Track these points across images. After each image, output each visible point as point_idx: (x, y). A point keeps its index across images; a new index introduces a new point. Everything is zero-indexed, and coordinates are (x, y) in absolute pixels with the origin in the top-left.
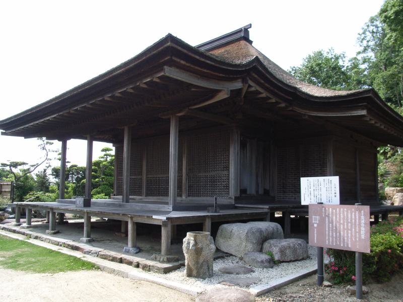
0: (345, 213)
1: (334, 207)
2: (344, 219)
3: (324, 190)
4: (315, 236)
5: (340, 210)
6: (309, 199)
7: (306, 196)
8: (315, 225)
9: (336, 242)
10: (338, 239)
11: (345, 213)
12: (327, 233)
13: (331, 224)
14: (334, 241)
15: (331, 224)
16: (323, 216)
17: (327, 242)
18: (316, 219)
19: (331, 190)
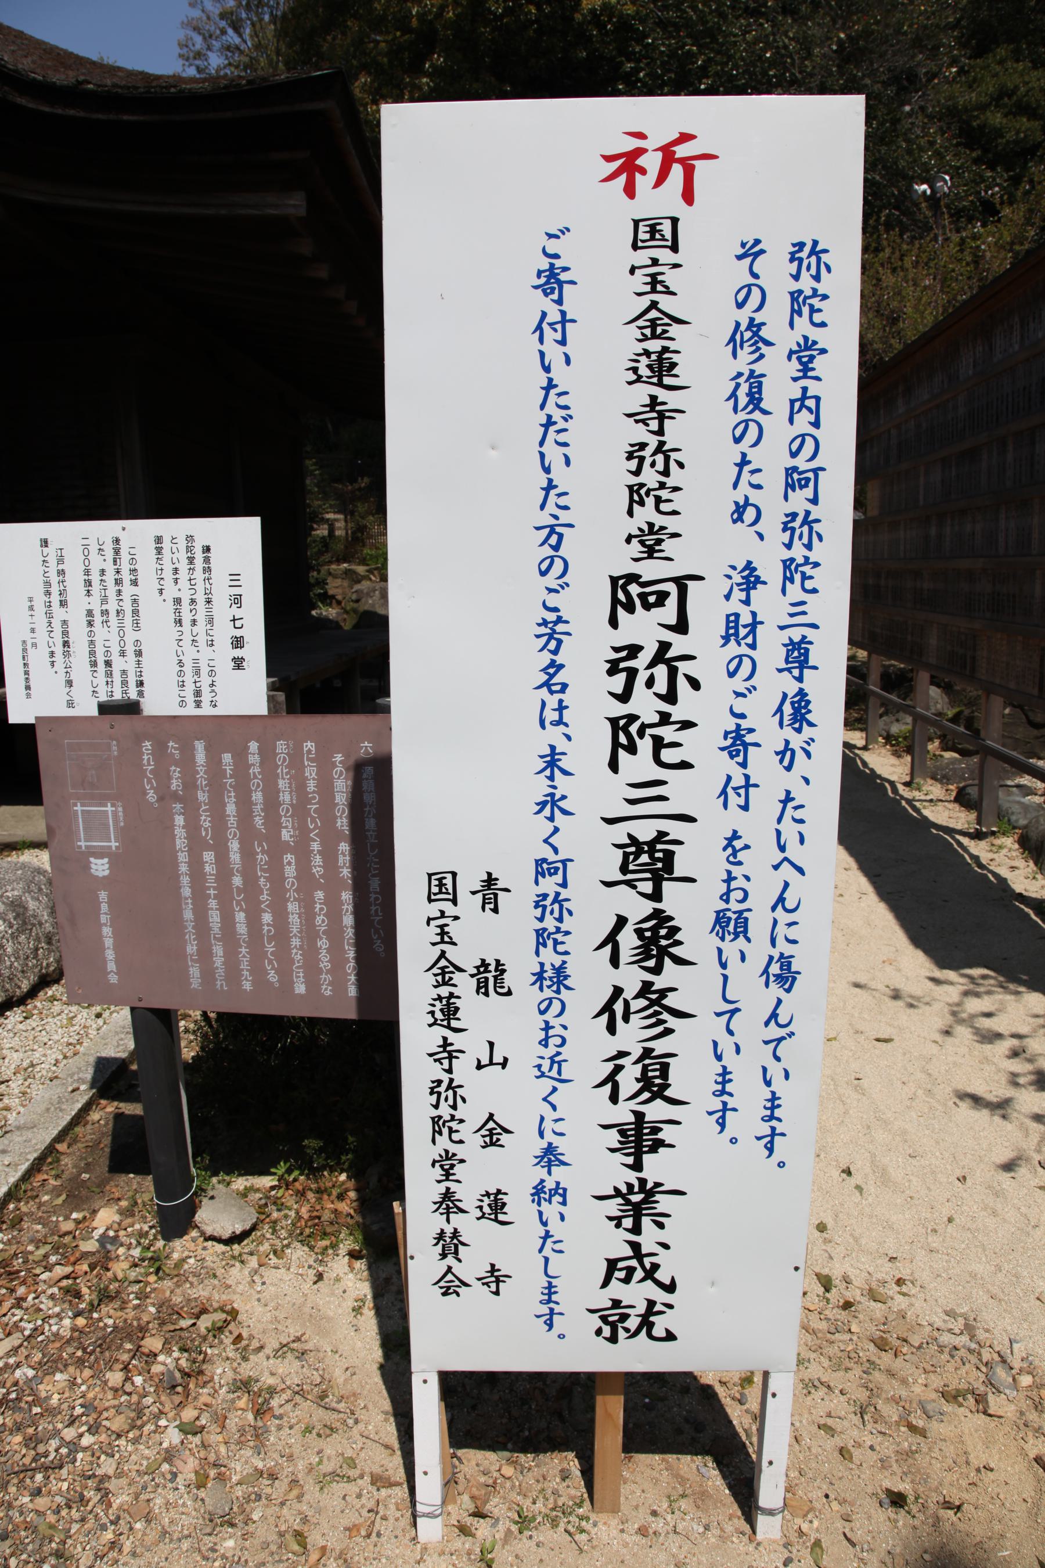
0: (311, 772)
1: (225, 731)
2: (300, 810)
3: (156, 614)
4: (109, 942)
5: (267, 754)
6: (62, 678)
7: (38, 658)
8: (100, 867)
9: (258, 971)
10: (270, 948)
11: (311, 772)
12: (188, 915)
13: (209, 856)
14: (244, 965)
15: (209, 856)
16: (152, 796)
17: (195, 971)
18: (96, 826)
19: (211, 621)
